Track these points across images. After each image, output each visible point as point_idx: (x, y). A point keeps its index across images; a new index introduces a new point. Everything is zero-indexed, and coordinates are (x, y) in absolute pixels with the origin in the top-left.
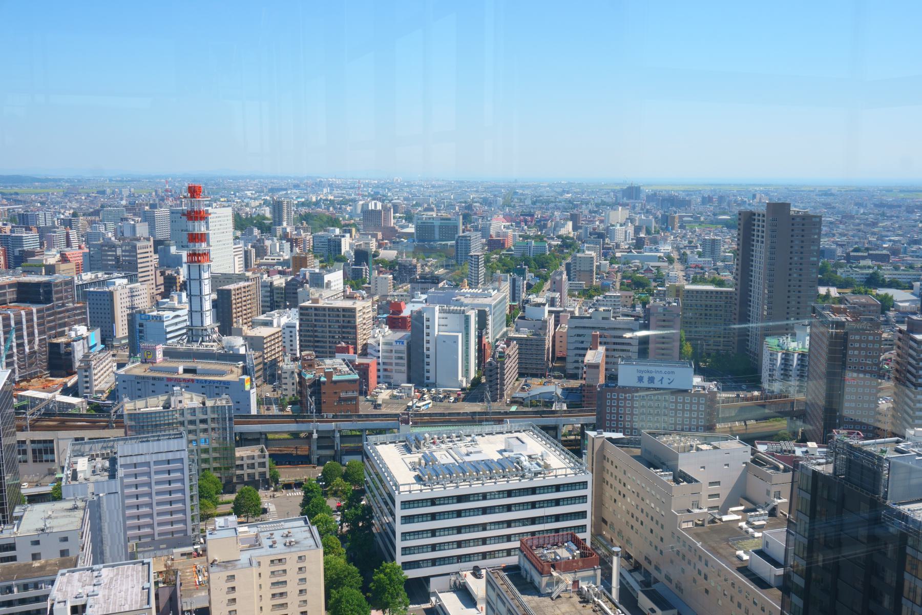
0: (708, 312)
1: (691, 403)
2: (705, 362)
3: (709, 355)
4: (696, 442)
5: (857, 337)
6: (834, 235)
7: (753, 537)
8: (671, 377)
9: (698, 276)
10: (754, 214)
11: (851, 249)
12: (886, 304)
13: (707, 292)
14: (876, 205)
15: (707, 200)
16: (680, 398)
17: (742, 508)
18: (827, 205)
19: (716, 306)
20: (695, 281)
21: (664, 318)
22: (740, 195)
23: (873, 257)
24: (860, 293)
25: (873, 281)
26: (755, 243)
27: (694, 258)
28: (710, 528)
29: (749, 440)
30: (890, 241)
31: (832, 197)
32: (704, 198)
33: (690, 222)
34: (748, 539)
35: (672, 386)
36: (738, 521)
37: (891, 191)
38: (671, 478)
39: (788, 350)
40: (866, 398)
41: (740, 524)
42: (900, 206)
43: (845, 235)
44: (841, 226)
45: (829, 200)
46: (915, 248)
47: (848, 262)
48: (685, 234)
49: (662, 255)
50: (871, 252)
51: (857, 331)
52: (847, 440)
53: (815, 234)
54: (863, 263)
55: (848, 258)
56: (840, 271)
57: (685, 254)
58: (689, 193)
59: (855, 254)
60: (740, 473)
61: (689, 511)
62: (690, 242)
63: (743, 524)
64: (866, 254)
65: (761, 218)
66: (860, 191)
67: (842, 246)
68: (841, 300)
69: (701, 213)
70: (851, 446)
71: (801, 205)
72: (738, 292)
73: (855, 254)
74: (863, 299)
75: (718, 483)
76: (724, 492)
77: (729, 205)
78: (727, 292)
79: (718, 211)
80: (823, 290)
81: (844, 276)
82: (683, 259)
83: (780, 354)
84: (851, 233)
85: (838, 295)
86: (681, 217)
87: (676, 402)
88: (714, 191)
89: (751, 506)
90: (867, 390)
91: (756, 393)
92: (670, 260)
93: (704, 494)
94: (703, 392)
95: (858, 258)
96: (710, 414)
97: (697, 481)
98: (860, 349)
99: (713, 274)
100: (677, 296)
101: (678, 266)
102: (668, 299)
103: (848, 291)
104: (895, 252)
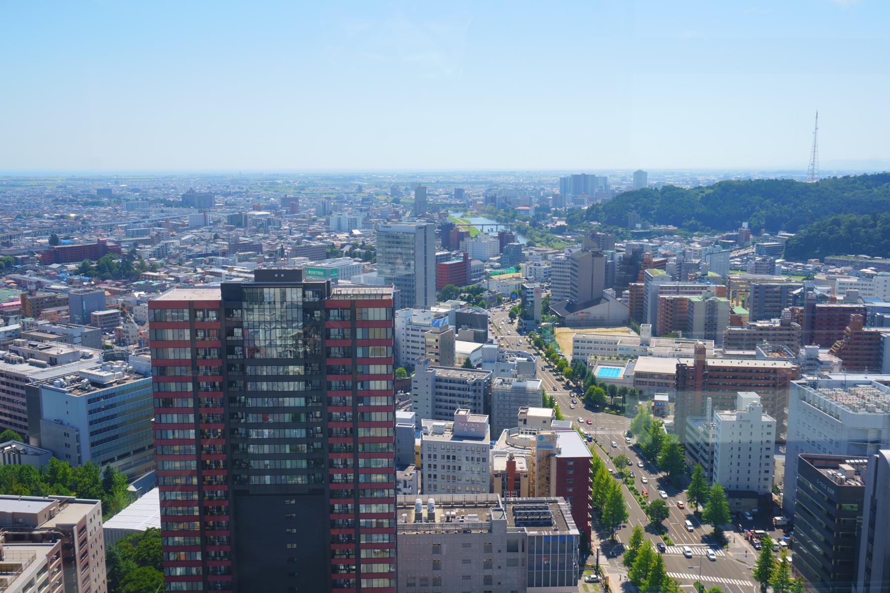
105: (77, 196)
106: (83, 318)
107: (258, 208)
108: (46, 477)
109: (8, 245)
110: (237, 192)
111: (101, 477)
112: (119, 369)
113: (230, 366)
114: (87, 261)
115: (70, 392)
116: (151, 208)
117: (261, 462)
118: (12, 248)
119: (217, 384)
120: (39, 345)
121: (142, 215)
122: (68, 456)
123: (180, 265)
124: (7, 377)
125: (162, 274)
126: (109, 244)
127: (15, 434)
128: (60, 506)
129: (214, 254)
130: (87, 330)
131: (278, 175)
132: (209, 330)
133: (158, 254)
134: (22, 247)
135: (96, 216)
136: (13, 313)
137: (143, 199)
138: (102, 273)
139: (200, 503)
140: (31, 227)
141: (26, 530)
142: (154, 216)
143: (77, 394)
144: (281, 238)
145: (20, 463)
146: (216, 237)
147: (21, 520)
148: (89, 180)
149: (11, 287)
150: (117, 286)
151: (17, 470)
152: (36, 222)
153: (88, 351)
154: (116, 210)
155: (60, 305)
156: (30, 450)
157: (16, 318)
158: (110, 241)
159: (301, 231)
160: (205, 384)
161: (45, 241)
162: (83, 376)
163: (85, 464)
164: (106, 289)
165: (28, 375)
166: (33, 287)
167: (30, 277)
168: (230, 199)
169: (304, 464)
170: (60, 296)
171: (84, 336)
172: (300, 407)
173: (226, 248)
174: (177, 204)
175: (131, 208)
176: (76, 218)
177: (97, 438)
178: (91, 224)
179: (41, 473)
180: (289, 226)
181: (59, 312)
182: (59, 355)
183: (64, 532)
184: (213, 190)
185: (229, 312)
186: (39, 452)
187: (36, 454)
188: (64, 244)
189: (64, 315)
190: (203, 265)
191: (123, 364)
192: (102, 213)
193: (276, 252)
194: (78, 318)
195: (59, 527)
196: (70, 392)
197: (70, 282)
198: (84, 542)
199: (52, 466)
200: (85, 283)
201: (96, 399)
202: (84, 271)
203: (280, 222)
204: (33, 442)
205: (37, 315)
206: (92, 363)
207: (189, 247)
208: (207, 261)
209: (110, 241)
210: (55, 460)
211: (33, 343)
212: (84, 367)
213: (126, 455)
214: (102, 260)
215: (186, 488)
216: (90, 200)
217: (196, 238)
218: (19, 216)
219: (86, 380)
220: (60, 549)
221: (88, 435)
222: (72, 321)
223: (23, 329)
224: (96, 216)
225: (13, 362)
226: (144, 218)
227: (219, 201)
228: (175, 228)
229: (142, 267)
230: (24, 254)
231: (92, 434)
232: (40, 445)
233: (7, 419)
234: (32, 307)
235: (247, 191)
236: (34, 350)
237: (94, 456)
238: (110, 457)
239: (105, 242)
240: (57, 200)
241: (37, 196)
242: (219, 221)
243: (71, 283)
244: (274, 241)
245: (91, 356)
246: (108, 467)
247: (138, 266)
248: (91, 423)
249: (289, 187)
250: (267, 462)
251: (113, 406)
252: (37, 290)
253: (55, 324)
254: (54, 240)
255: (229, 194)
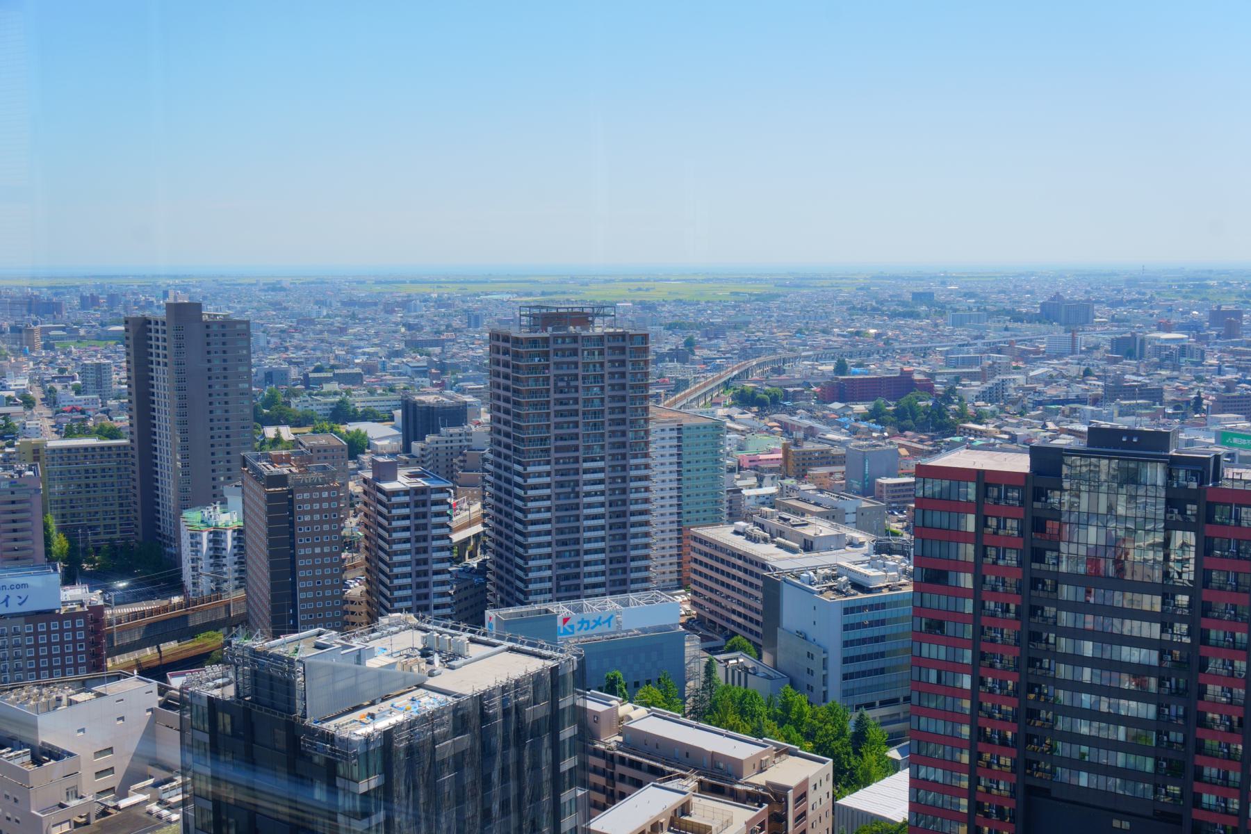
0: (91, 481)
1: (61, 631)
2: (91, 561)
3: (97, 550)
4: (66, 693)
5: (306, 496)
6: (287, 349)
7: (170, 822)
8: (23, 592)
9: (75, 425)
10: (150, 323)
11: (311, 368)
12: (356, 447)
13: (86, 449)
14: (344, 304)
15: (89, 302)
16: (42, 627)
17: (150, 781)
18: (276, 305)
19: (103, 470)
20: (69, 434)
21: (13, 498)
22: (144, 293)
23: (340, 379)
24: (323, 431)
25: (341, 413)
26: (154, 366)
27: (67, 396)
28: (100, 825)
29: (155, 672)
30: (364, 354)
31: (283, 293)
32: (83, 298)
33: (61, 338)
34: (161, 827)
35: (27, 608)
36: (146, 802)
37: (364, 282)
38: (28, 758)
39: (216, 526)
40: (328, 582)
41: (149, 807)
42: (375, 304)
43: (303, 348)
44: (297, 335)
45: (279, 297)
46: (396, 361)
47: (307, 387)
48: (54, 358)
49: (13, 394)
50: (337, 371)
51: (306, 486)
52: (249, 643)
53: (243, 348)
54: (327, 387)
55: (306, 381)
56: (294, 401)
57: (52, 391)
58: (57, 290)
59: (316, 375)
60: (143, 727)
61: (62, 806)
62: (62, 371)
63: (154, 808)
64: (330, 375)
65: (159, 327)
66: (322, 283)
67: (297, 364)
68: (296, 443)
69: (80, 324)
70: (254, 652)
71: (238, 306)
72: (136, 445)
73: (316, 375)
74: (322, 440)
75: (110, 750)
76: (121, 763)
77: (125, 308)
78: (118, 447)
79: (108, 319)
80: (270, 432)
81: (300, 409)
82: (51, 399)
83: (205, 535)
84: (310, 345)
85: (292, 437)
86: (45, 331)
87: (36, 634)
88: (102, 286)
89: (165, 775)
90: (328, 571)
91: (176, 600)
92: (28, 403)
93: (87, 774)
94: (79, 610)
95: (320, 381)
96: (96, 643)
97: (70, 754)
98: (312, 512)
99: (102, 419)
100: (36, 459)
101: (41, 410)
102: (18, 467)
103: (307, 430)
104: (369, 369)
105: (882, 303)
106: (863, 485)
107: (1167, 328)
108: (775, 713)
109: (779, 371)
110: (1134, 301)
111: (850, 729)
112: (894, 568)
113: (1035, 582)
114: (881, 401)
115: (821, 592)
116: (989, 324)
117: (1075, 747)
118: (783, 377)
119: (1012, 607)
120: (794, 519)
121: (975, 333)
122: (810, 688)
123: (1022, 415)
124: (745, 560)
125: (991, 428)
126: (917, 377)
127: (747, 644)
128: (777, 756)
129: (1081, 400)
130: (865, 505)
131: (1210, 271)
132: (1005, 519)
133: (988, 396)
134: (797, 376)
135: (905, 334)
136: (771, 470)
137: (979, 309)
138: (903, 421)
139: (971, 793)
140: (813, 347)
141: (726, 781)
142: (992, 336)
143: (829, 597)
144: (1199, 379)
145: (746, 686)
146: (1087, 373)
147: (721, 765)
148: (903, 279)
149: (773, 433)
150: (921, 441)
151: (739, 694)
152: (821, 339)
153: (859, 536)
154: (936, 325)
155: (834, 464)
156: (761, 670)
157: (773, 478)
158: (921, 373)
159: (1240, 369)
160: (992, 605)
161: (829, 367)
162: (840, 571)
163: (830, 703)
164: (901, 446)
165: (771, 562)
166: (800, 435)
167: (801, 420)
168: (1122, 311)
169: (1149, 765)
170: (837, 451)
171: (860, 512)
172: (1149, 666)
173: (1100, 391)
174: (1031, 318)
175: (959, 322)
176: (877, 336)
177: (853, 667)
178: (896, 345)
179: (769, 706)
180: (1219, 359)
181: (831, 474)
182: (816, 537)
183: (775, 795)
184: (1094, 295)
185: (1039, 494)
186: (772, 675)
187: (768, 677)
188: (855, 374)
189: (838, 480)
190: (1059, 417)
191: (903, 561)
192: (915, 331)
193: (1188, 403)
194: (857, 485)
195: (770, 786)
196: (821, 592)
197: (854, 432)
198: (802, 816)
199: (785, 697)
200: (875, 435)
201: (860, 608)
202: (875, 415)
203: (1203, 352)
204: (767, 658)
205: (801, 476)
206: (857, 554)
207: (1040, 387)
208: (1067, 412)
209: (921, 373)
210: (790, 690)
211: (785, 515)
212: (846, 559)
213: (893, 702)
214: (904, 401)
215: (951, 766)
216: (901, 309)
217: (1054, 374)
218: (800, 331)
219: (845, 578)
220: (766, 818)
221: (839, 661)
222: (848, 489)
223: (781, 493)
224: (905, 334)
225: (754, 540)
226: (976, 338)
227: (1101, 314)
228: (1023, 356)
229: (962, 415)
230: (798, 385)
231: (846, 660)
232: (775, 667)
233: (740, 620)
234: (797, 465)
235: (1152, 298)
236: (786, 527)
237: (846, 694)
238: (869, 700)
239: (911, 373)
240: (854, 308)
241: (828, 301)
242: (1097, 347)
243: (855, 433)
244: (1186, 383)
245: (861, 544)
246: (861, 715)
247: (956, 414)
248: (847, 644)
249: (1230, 292)
250: (1085, 749)
251: (882, 622)
252: (806, 439)
253: (821, 491)
254: (841, 368)
255: (1121, 303)
